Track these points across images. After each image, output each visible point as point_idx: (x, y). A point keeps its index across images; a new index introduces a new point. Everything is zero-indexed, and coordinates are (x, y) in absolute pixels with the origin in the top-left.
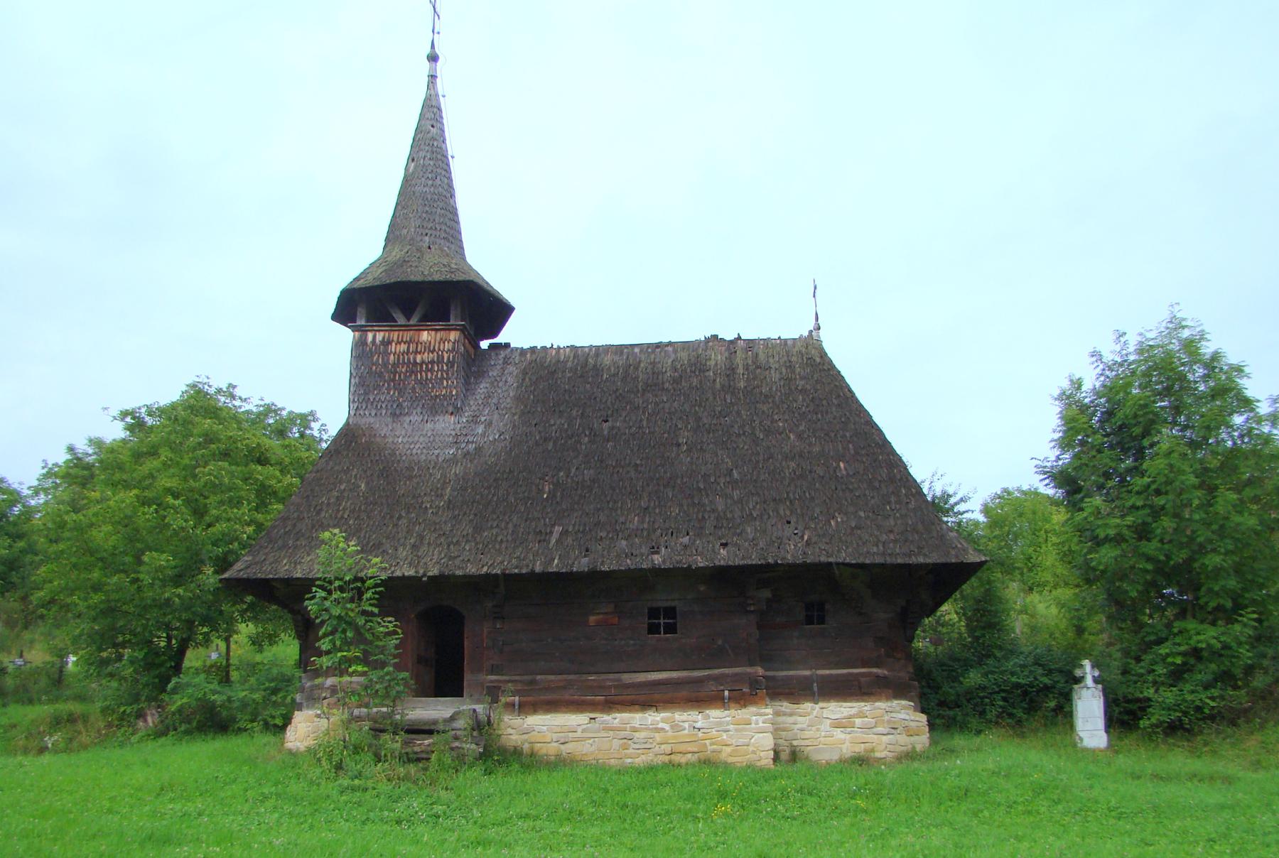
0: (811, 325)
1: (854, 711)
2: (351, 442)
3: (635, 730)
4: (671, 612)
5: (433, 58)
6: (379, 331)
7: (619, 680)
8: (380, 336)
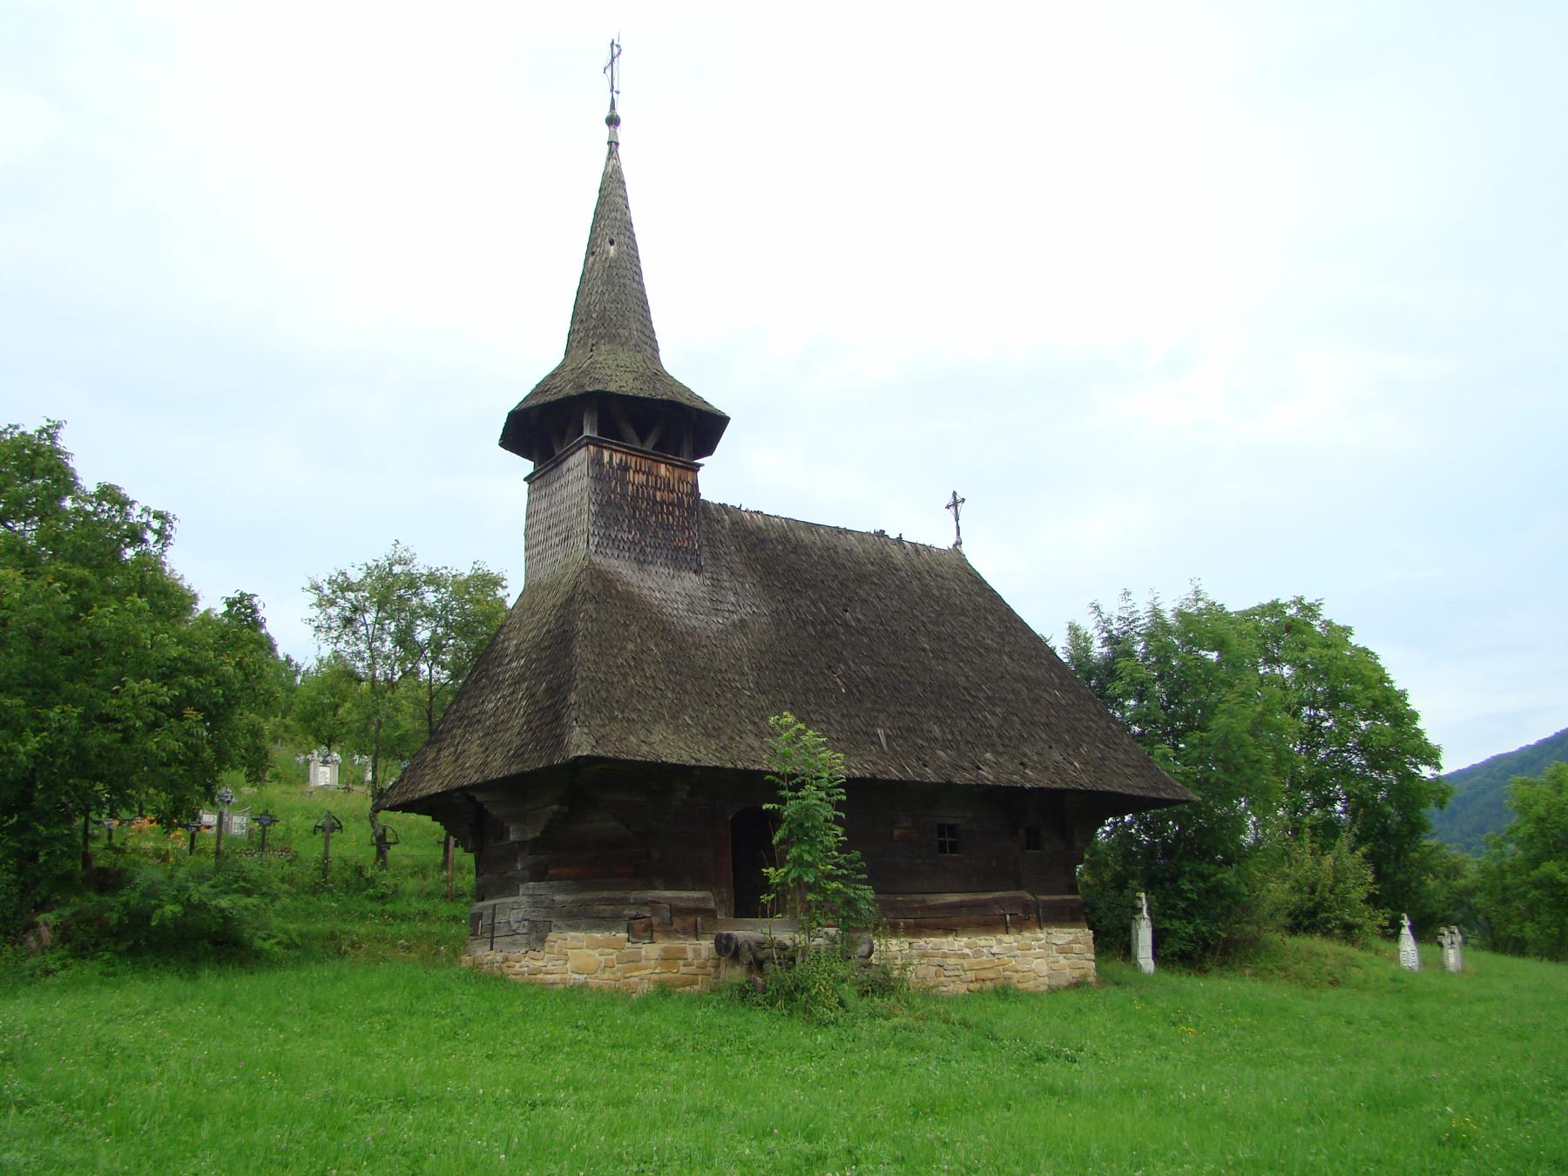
0: (953, 540)
1: (1071, 937)
2: (610, 591)
3: (945, 956)
4: (952, 830)
5: (613, 121)
6: (616, 451)
7: (924, 901)
8: (617, 458)
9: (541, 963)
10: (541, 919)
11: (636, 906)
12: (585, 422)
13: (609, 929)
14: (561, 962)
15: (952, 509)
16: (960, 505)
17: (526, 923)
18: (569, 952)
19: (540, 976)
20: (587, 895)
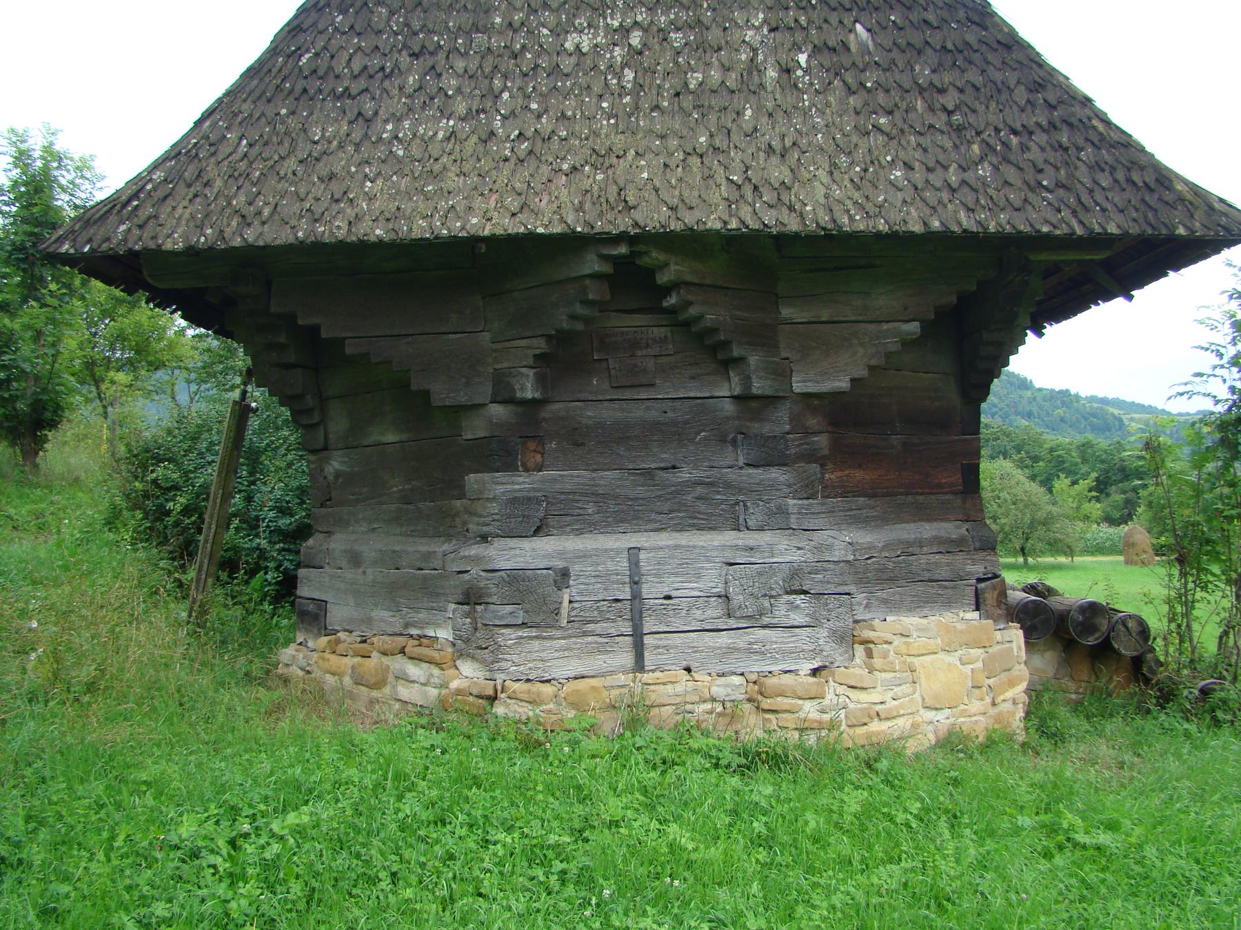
9: (874, 697)
10: (832, 588)
11: (981, 554)
13: (948, 604)
14: (906, 688)
17: (798, 599)
18: (915, 660)
19: (875, 726)
20: (908, 531)
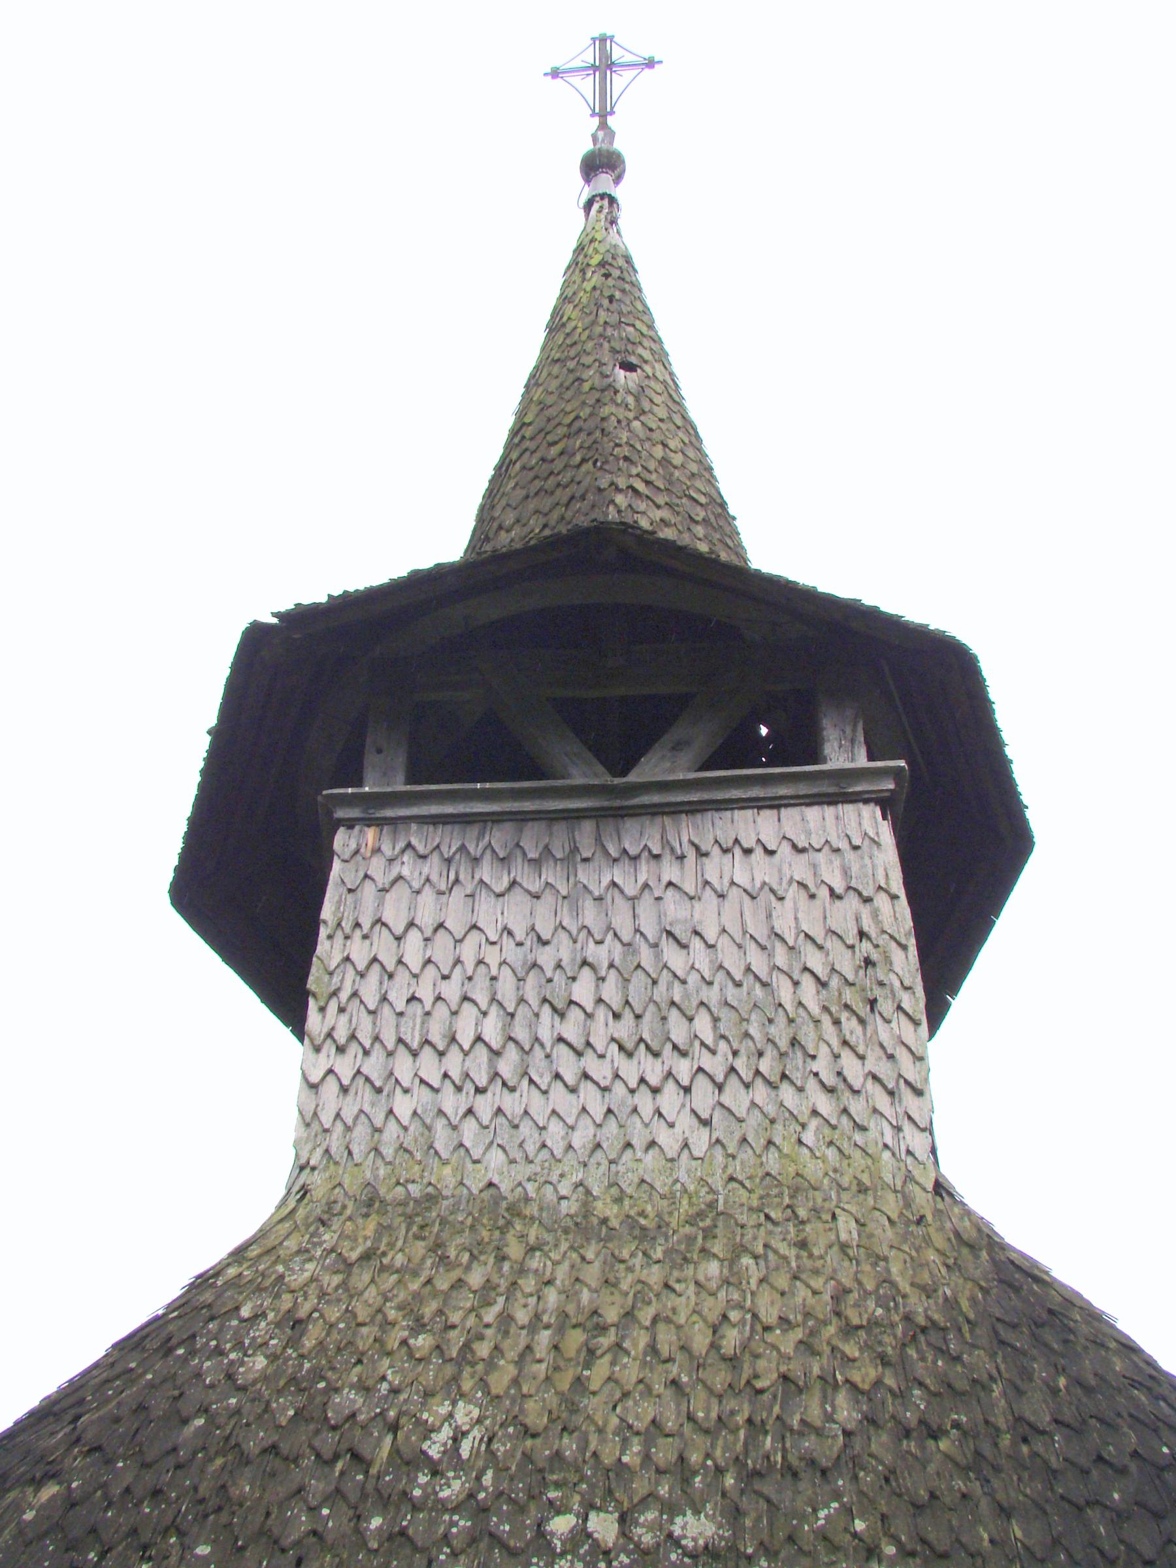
12: (826, 723)
15: (587, 85)
16: (618, 81)
